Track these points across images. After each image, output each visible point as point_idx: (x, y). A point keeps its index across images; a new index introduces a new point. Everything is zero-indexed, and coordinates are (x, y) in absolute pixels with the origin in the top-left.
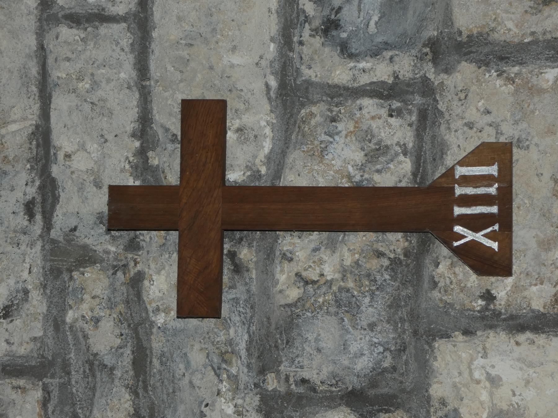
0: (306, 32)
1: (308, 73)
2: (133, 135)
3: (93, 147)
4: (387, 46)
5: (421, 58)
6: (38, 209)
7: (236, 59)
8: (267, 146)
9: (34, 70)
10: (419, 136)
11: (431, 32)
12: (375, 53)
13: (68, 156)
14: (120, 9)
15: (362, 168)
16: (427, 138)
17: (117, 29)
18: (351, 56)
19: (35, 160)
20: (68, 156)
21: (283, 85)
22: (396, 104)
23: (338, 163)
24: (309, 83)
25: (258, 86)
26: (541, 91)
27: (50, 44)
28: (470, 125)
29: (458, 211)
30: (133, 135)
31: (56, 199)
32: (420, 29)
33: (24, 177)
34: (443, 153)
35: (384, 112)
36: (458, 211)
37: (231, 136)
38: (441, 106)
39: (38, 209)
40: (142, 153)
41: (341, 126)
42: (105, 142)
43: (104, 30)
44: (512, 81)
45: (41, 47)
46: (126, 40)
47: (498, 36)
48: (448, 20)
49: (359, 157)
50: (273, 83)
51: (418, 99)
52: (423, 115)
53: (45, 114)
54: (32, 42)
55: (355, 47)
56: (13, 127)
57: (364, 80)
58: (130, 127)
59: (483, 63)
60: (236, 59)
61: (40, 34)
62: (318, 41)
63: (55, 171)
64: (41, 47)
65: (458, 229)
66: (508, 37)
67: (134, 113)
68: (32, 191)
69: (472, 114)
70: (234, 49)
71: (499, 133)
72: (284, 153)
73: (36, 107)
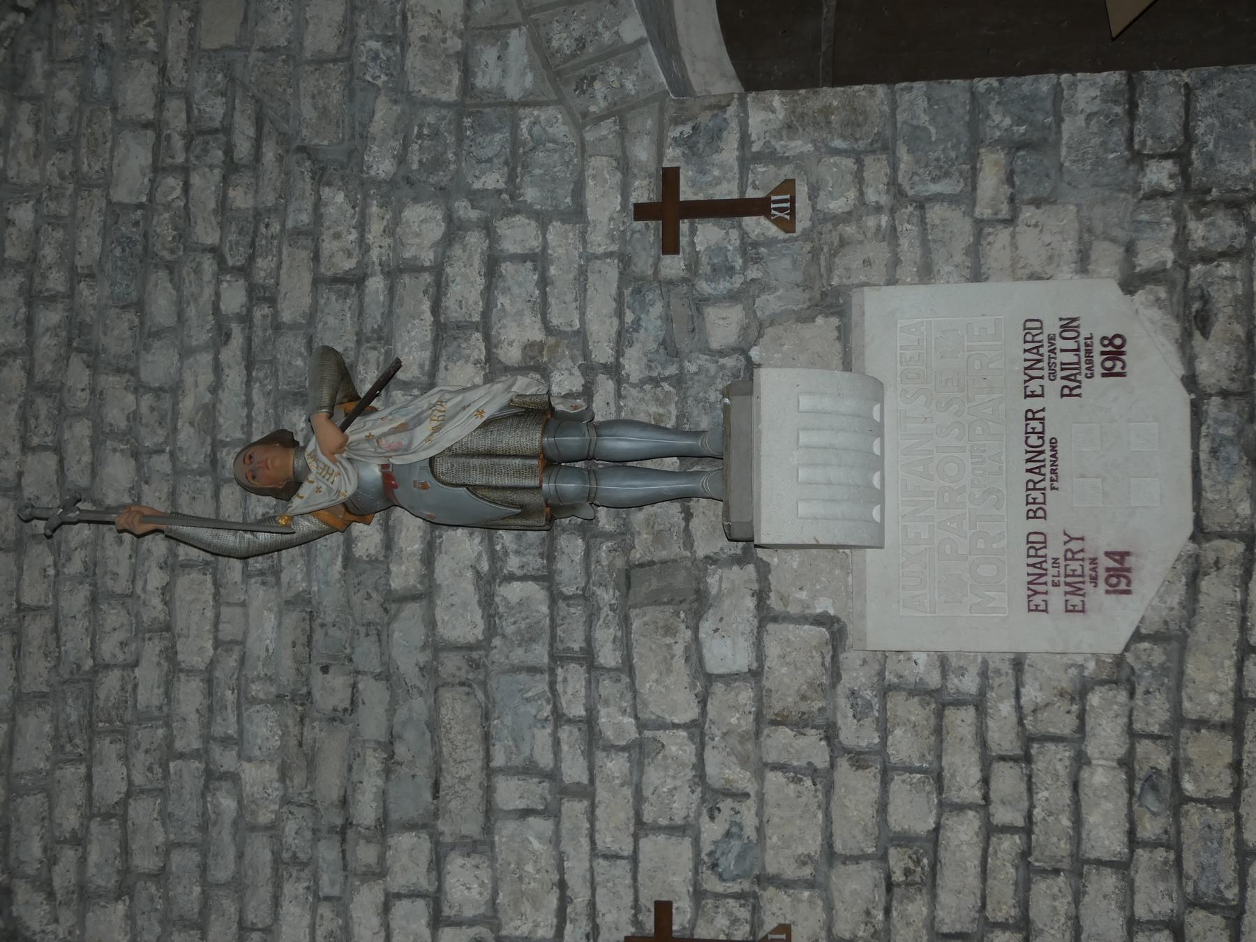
0: (704, 868)
1: (705, 886)
2: (632, 908)
3: (614, 912)
4: (738, 876)
5: (753, 883)
6: (591, 937)
7: (675, 879)
8: (689, 916)
9: (588, 876)
10: (753, 916)
11: (756, 872)
12: (734, 880)
13: (603, 915)
14: (625, 854)
15: (729, 928)
16: (756, 916)
17: (624, 862)
18: (724, 880)
19: (589, 915)
20: (603, 915)
21: (695, 890)
22: (743, 902)
23: (719, 926)
24: (706, 891)
25: (685, 890)
26: (802, 901)
27: (595, 864)
28: (774, 914)
29: (773, 206)
30: (632, 908)
31: (599, 933)
32: (751, 869)
33: (584, 922)
34: (762, 925)
35: (738, 905)
36: (773, 206)
37: (674, 911)
38: (762, 904)
39: (591, 937)
40: (635, 915)
41: (720, 910)
42: (490, 358)
43: (619, 862)
44: (789, 896)
45: (591, 867)
46: (628, 867)
47: (785, 877)
48: (764, 868)
49: (727, 923)
50: (691, 889)
51: (752, 900)
52: (754, 908)
53: (593, 895)
54: (587, 864)
55: (725, 876)
56: (579, 900)
57: (729, 891)
58: (630, 904)
59: (778, 887)
60: (675, 879)
61: (591, 861)
62: (709, 872)
63: (598, 921)
64: (591, 867)
65: (773, 212)
66: (789, 878)
67: (631, 898)
68: (588, 929)
69: (774, 909)
70: (674, 874)
71: (785, 918)
72: (696, 920)
73: (589, 893)
